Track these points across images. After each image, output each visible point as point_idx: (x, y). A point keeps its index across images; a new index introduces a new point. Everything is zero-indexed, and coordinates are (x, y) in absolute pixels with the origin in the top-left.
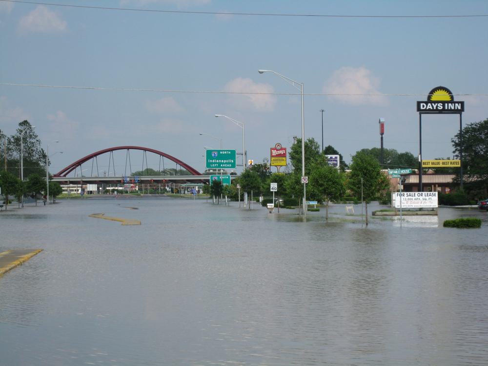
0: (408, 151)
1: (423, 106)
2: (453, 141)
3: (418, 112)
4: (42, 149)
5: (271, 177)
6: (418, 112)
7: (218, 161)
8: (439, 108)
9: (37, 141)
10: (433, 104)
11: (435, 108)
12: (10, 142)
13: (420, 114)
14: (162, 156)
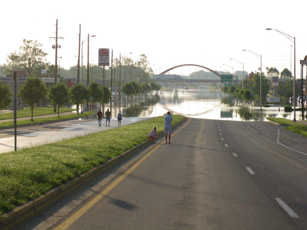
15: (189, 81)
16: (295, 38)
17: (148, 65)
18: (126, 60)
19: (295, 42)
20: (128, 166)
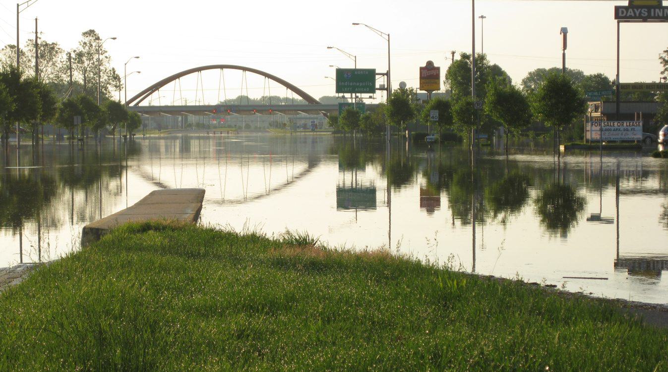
0: (433, 61)
1: (623, 12)
2: (661, 58)
3: (616, 20)
4: (113, 69)
5: (430, 102)
6: (616, 20)
7: (351, 84)
8: (643, 15)
9: (106, 57)
10: (635, 10)
11: (637, 15)
12: (70, 58)
13: (618, 23)
14: (267, 78)
15: (222, 109)
16: (389, 35)
17: (105, 62)
18: (42, 48)
19: (389, 41)
20: (121, 75)
